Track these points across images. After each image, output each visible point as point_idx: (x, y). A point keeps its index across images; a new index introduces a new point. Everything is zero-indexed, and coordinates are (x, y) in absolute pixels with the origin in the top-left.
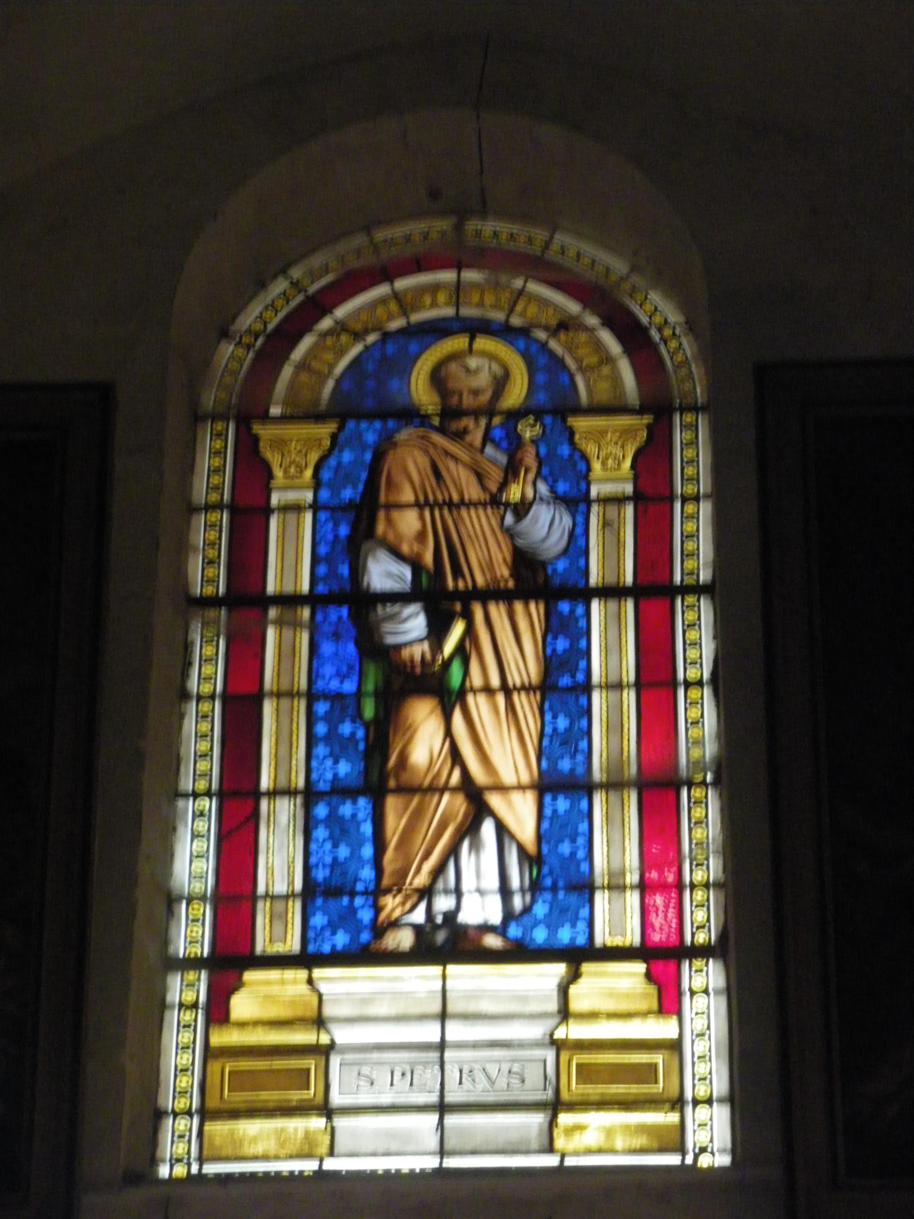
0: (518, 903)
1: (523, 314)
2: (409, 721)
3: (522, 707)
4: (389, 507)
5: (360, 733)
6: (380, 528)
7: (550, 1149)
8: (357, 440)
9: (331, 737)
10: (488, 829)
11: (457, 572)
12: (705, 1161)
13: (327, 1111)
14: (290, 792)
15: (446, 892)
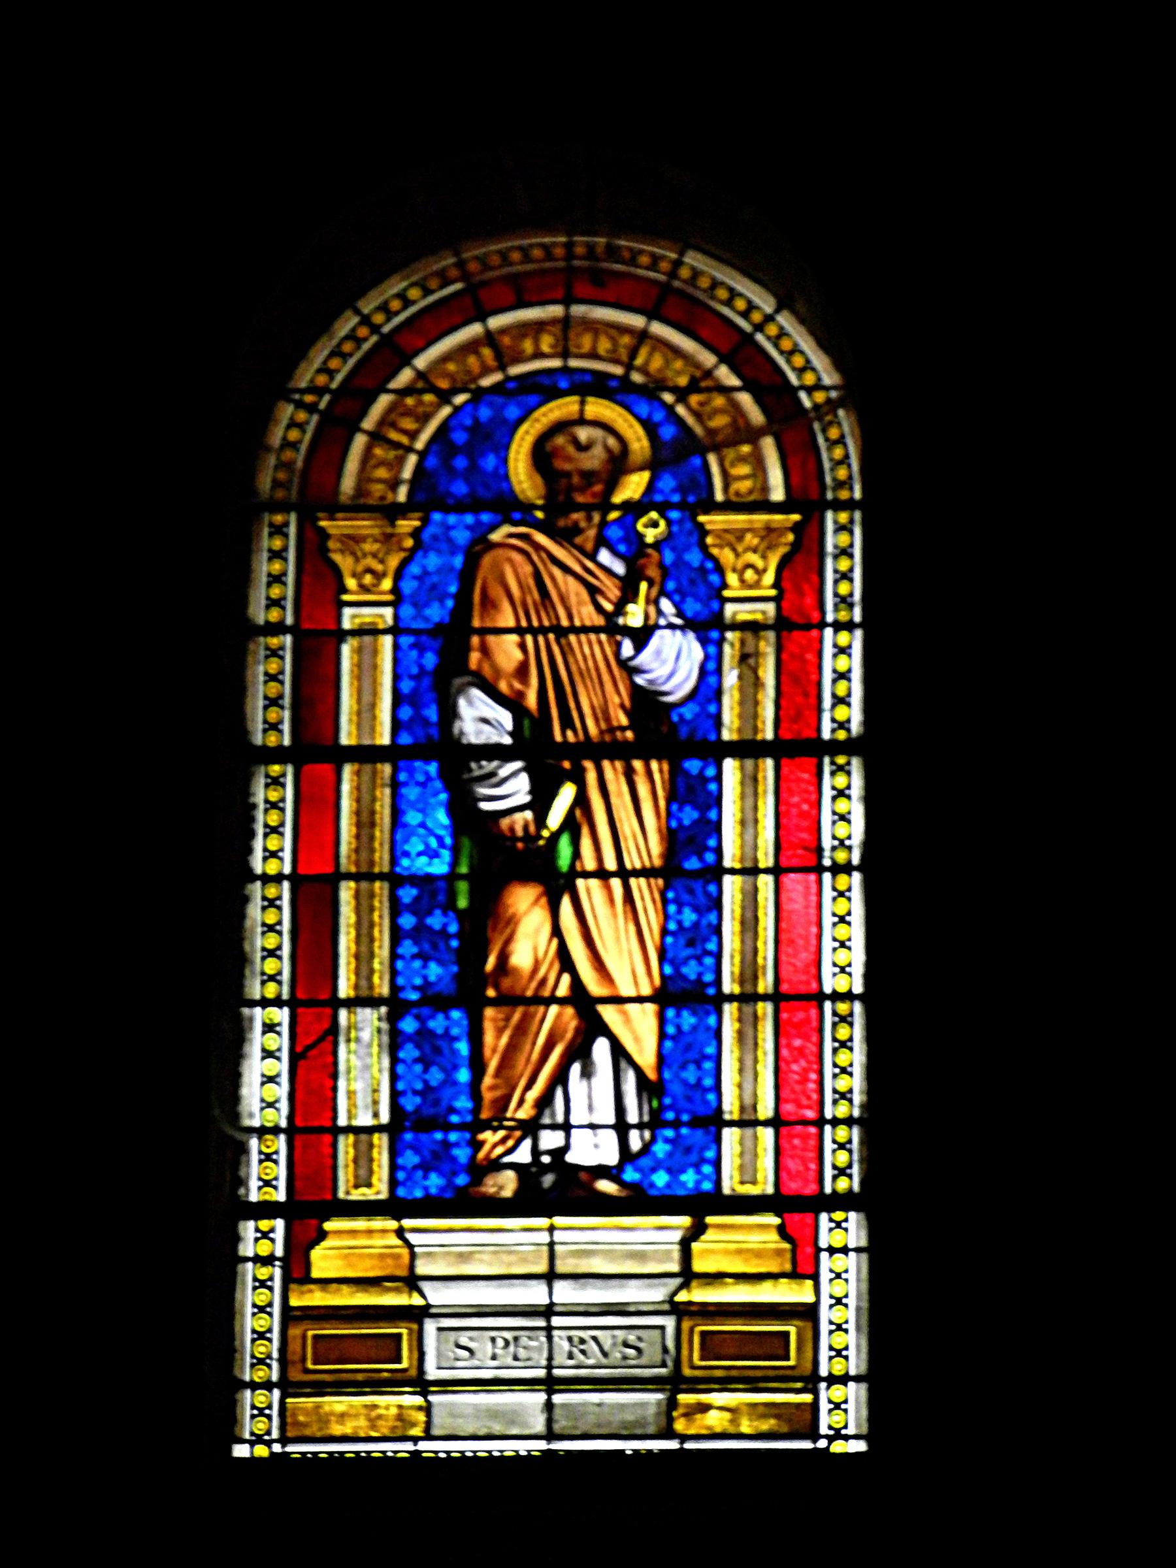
0: (635, 1141)
1: (643, 370)
2: (511, 911)
3: (643, 899)
4: (484, 632)
5: (453, 928)
6: (475, 657)
7: (668, 1433)
8: (444, 542)
9: (419, 933)
10: (601, 1049)
11: (567, 722)
12: (838, 1447)
13: (422, 1385)
14: (372, 1002)
15: (554, 1127)
